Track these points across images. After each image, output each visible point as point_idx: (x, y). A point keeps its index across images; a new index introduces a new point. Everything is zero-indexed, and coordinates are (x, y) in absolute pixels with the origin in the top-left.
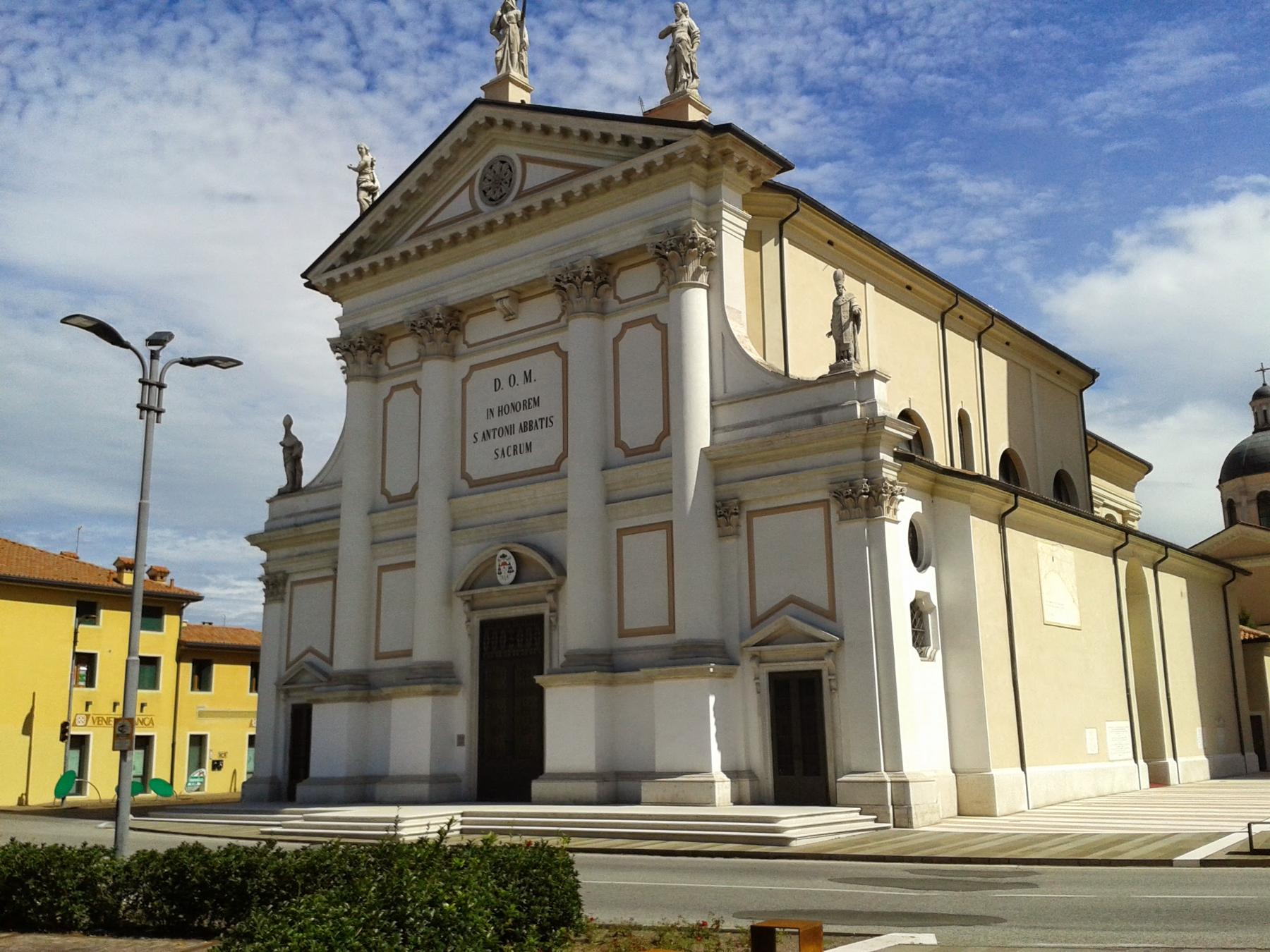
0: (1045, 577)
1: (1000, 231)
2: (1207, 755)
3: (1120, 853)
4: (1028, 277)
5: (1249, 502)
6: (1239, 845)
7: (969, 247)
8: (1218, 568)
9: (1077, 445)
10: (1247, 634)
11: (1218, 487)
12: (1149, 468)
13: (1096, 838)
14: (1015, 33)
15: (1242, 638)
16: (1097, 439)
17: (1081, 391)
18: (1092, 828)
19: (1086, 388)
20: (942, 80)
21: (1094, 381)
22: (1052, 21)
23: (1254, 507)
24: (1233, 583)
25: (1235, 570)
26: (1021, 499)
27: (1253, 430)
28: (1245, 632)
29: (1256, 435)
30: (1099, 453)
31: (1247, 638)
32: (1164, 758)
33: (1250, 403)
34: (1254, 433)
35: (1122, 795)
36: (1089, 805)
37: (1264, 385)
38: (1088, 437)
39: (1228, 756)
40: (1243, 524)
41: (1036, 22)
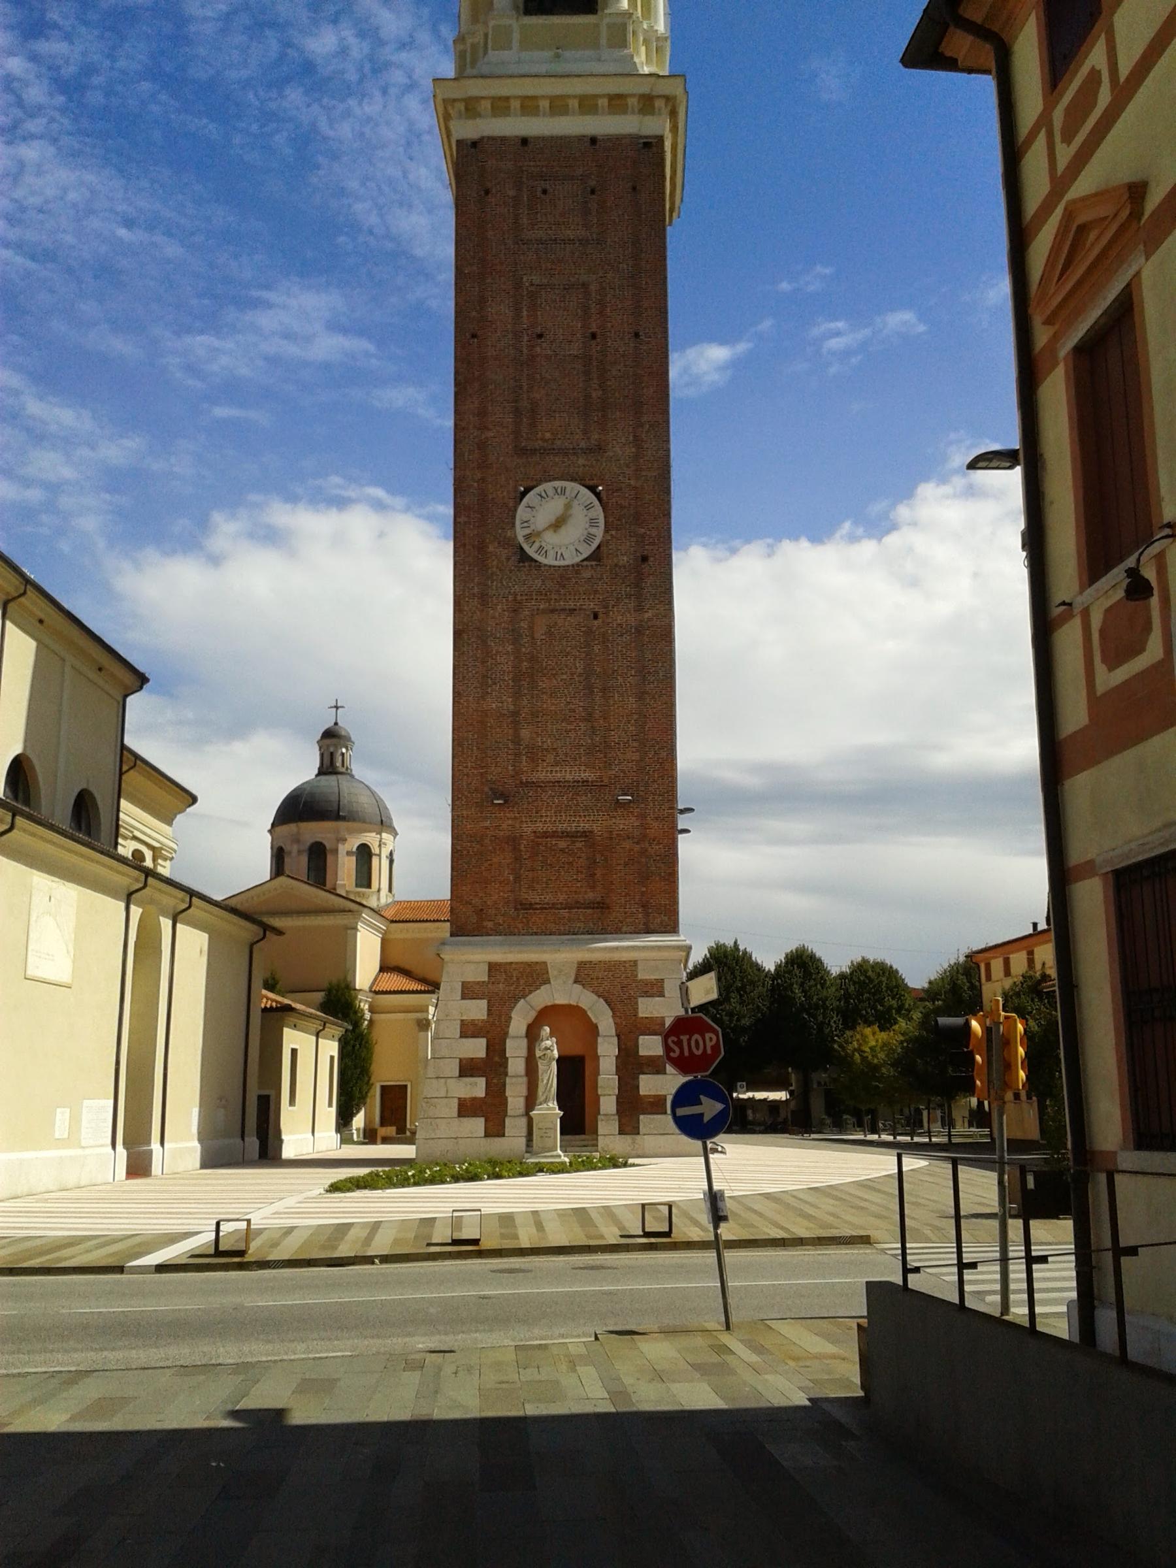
0: (36, 921)
1: (67, 473)
2: (200, 1140)
3: (66, 1259)
4: (101, 544)
5: (300, 852)
6: (205, 1247)
7: (27, 483)
8: (243, 923)
9: (110, 760)
10: (269, 1002)
11: (270, 831)
12: (194, 799)
13: (43, 1241)
14: (122, 232)
15: (263, 1006)
16: (137, 757)
17: (126, 696)
18: (39, 1229)
19: (132, 693)
20: (19, 260)
21: (141, 688)
22: (169, 234)
23: (304, 859)
24: (262, 942)
25: (266, 928)
26: (19, 820)
27: (316, 772)
28: (269, 998)
29: (319, 778)
30: (137, 774)
31: (268, 1006)
32: (149, 1143)
33: (318, 742)
34: (317, 776)
35: (89, 1188)
36: (46, 1201)
37: (336, 724)
38: (125, 752)
39: (227, 1141)
40: (289, 876)
41: (151, 228)
